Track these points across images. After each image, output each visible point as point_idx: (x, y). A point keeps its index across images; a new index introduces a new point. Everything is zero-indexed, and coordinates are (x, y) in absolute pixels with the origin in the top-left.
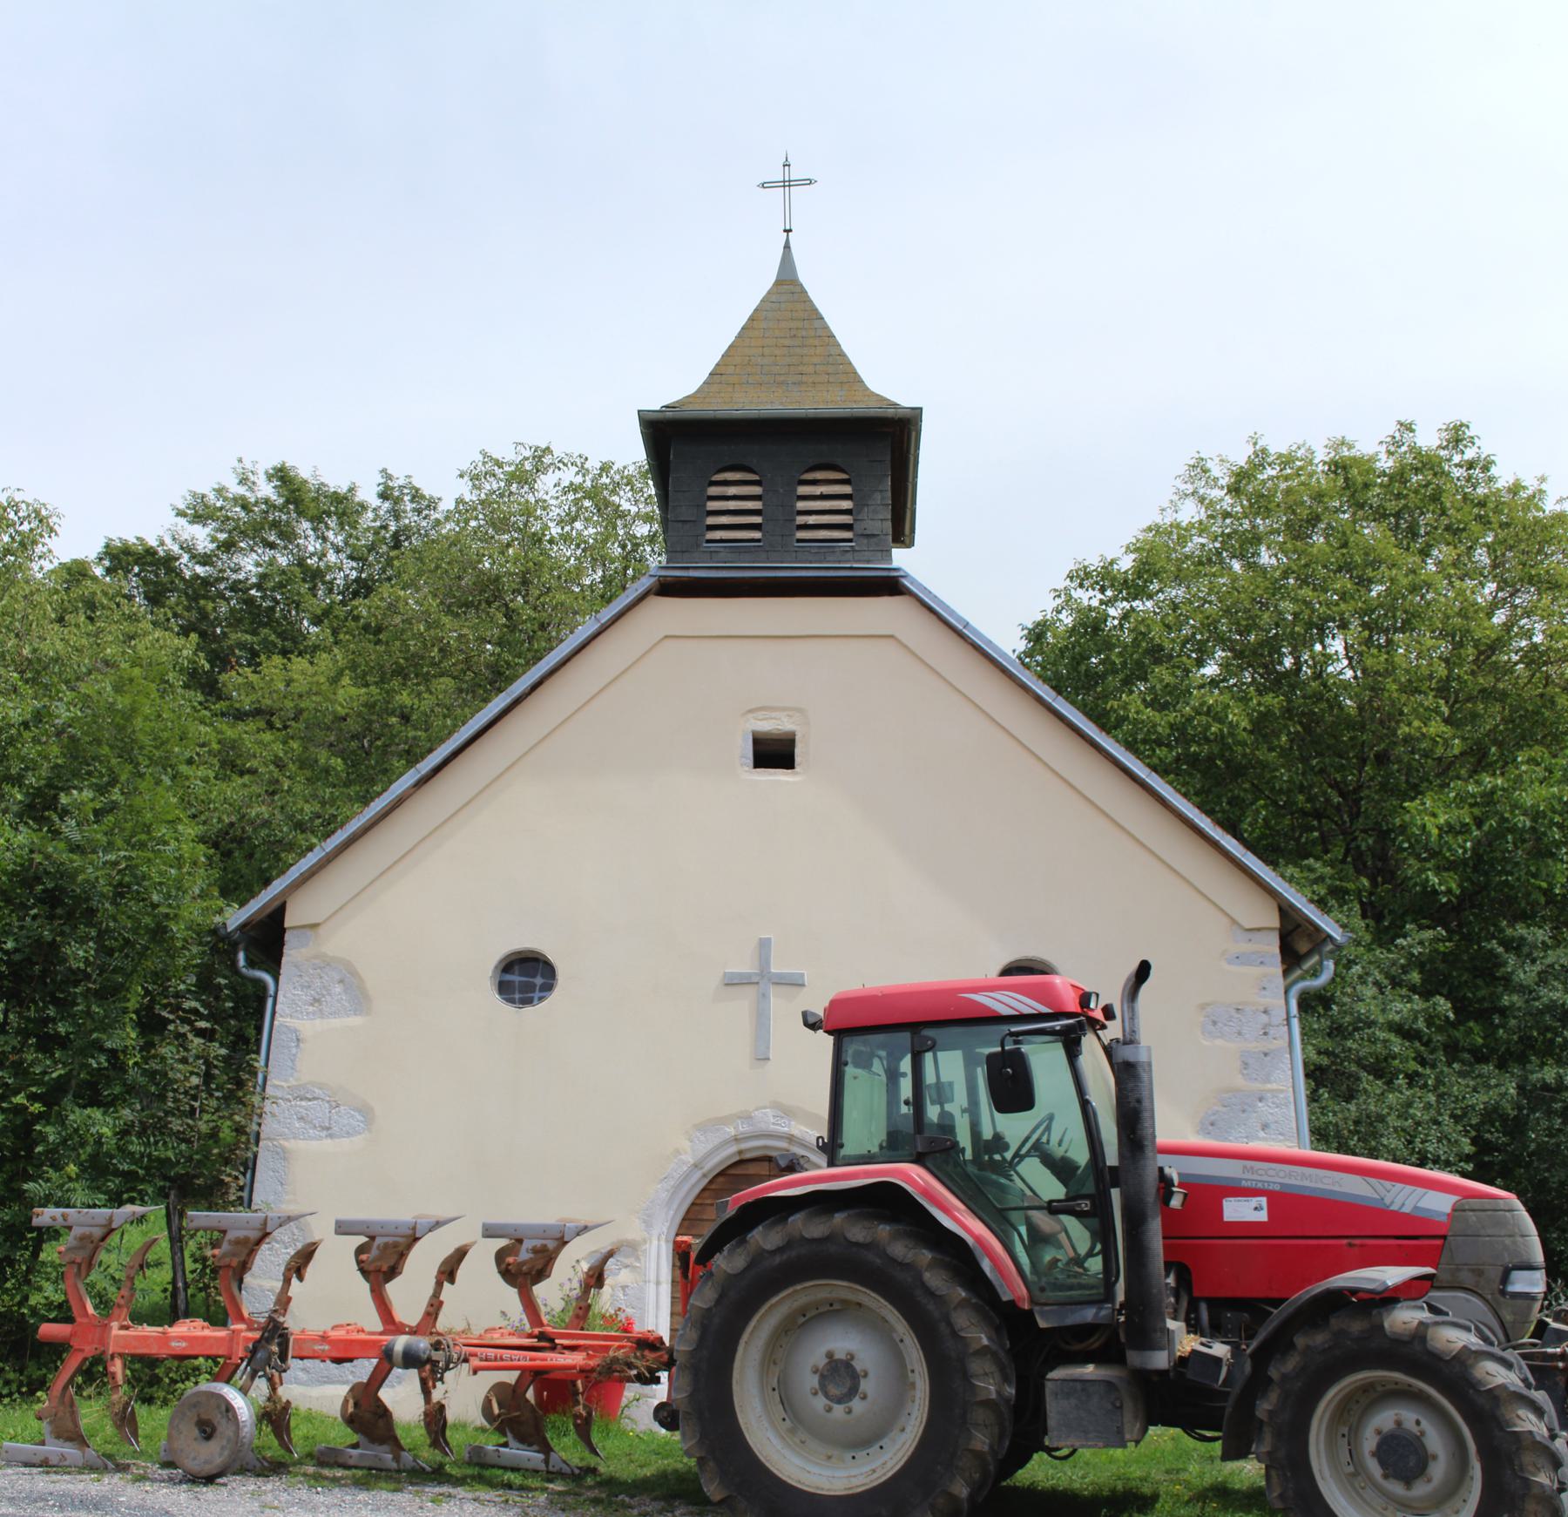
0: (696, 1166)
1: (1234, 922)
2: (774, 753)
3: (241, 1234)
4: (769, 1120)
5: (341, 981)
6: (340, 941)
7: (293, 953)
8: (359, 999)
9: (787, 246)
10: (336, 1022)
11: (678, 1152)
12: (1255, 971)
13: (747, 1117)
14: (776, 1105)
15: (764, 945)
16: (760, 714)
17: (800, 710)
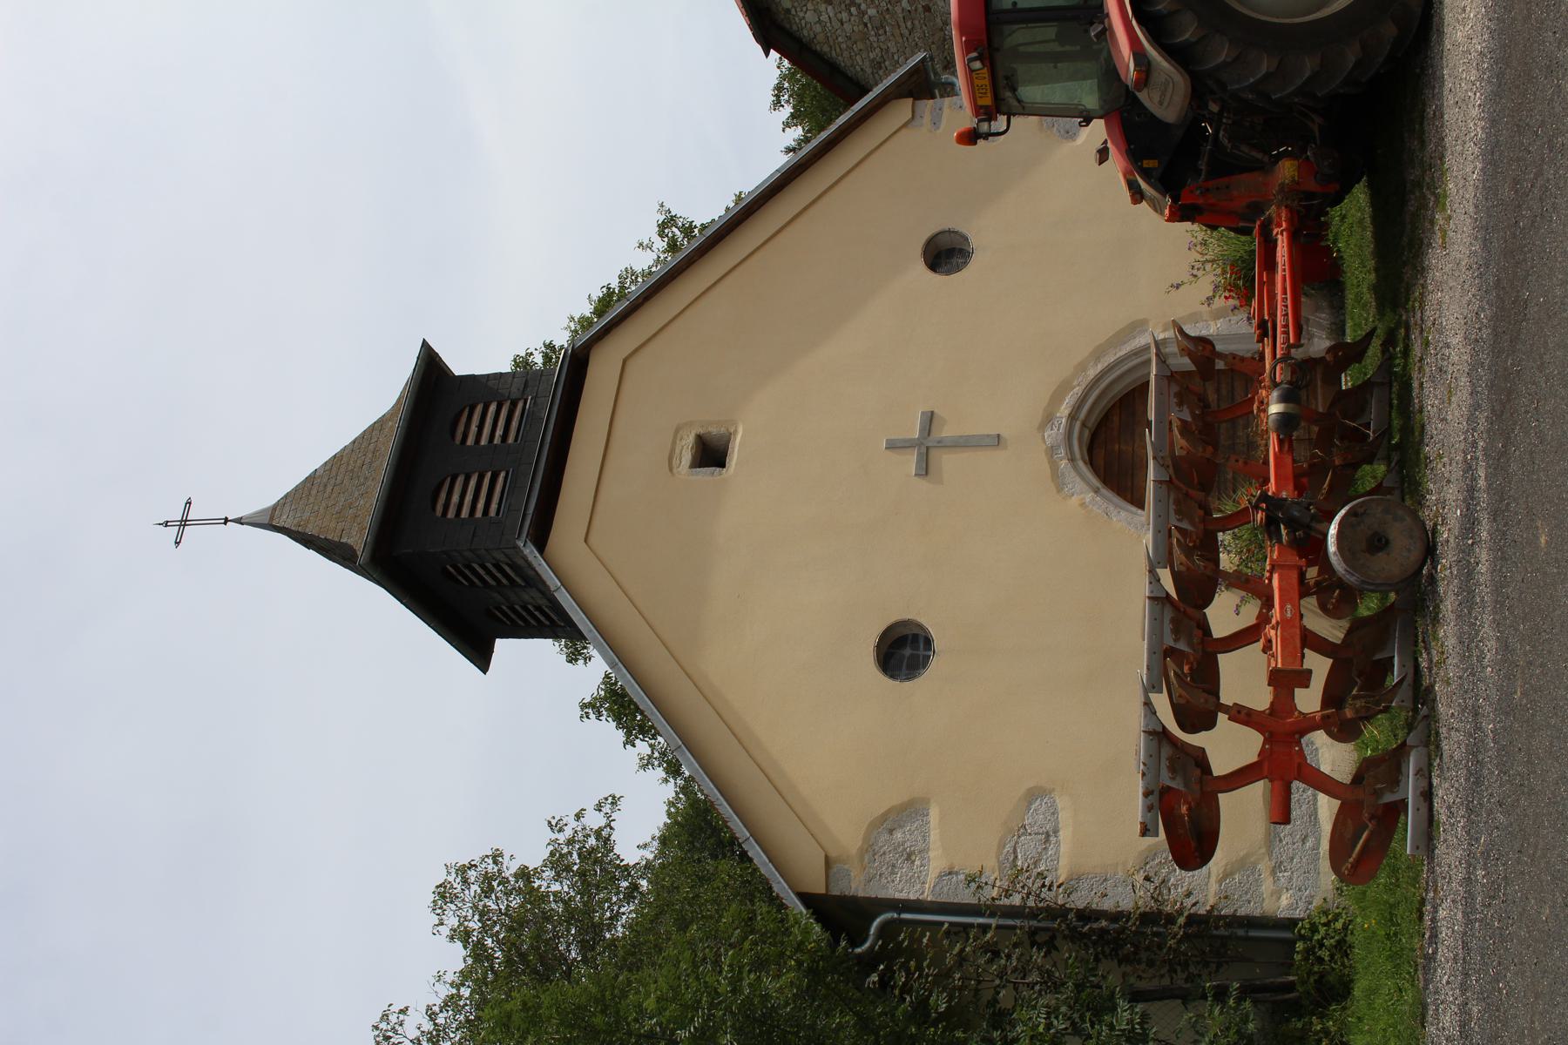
0: (1097, 491)
1: (905, 125)
2: (711, 454)
3: (1168, 627)
4: (1055, 434)
5: (891, 831)
6: (846, 835)
7: (857, 885)
8: (910, 811)
9: (239, 521)
10: (934, 836)
11: (1083, 505)
12: (946, 110)
13: (1051, 451)
14: (1042, 427)
15: (892, 446)
16: (675, 462)
17: (677, 431)
